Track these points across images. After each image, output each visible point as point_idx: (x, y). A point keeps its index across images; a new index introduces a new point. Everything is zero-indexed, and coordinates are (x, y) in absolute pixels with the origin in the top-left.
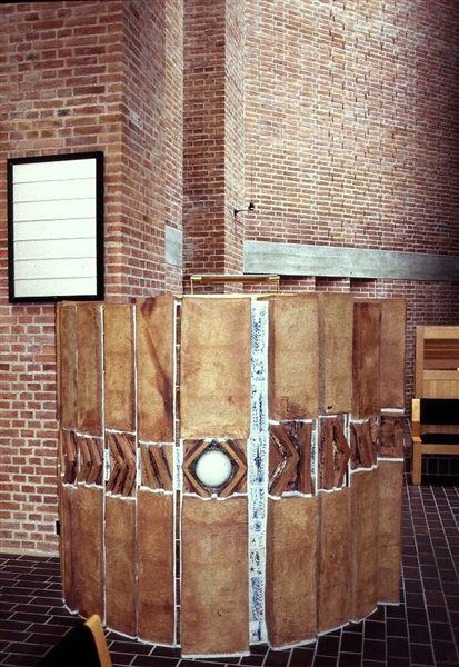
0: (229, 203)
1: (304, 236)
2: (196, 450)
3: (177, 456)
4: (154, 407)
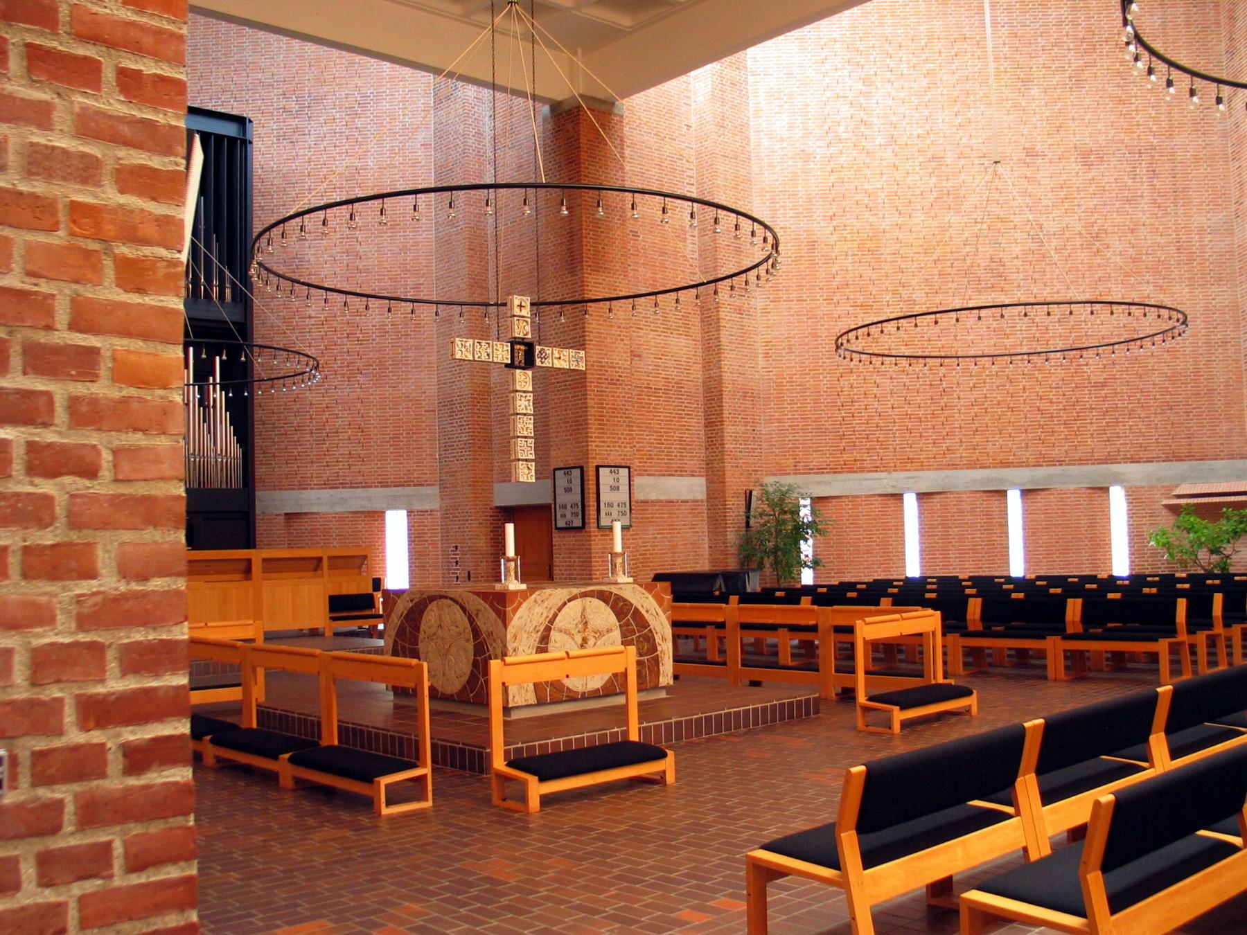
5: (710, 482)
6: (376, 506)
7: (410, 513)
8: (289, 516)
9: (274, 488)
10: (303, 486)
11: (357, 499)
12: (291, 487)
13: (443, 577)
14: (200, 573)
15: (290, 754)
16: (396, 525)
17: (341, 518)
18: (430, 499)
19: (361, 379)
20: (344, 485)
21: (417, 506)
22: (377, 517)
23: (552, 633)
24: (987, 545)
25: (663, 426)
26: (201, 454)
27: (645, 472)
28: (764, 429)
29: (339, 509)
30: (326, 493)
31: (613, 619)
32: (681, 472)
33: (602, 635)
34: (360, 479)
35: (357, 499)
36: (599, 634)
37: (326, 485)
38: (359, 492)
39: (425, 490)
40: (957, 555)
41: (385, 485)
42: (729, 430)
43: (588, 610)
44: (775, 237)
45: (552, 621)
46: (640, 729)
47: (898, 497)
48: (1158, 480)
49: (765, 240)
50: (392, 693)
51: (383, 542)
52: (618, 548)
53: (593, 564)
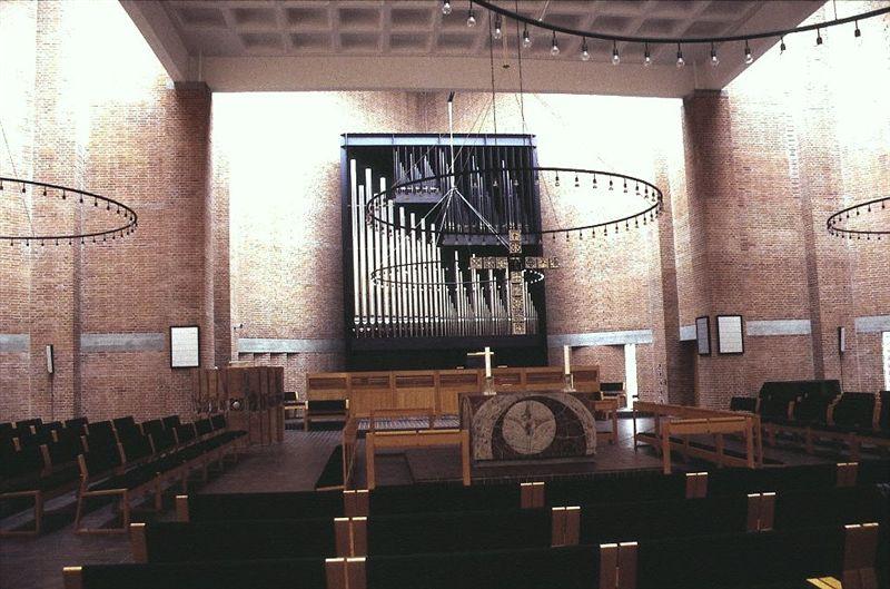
0: (232, 325)
1: (265, 335)
2: (232, 401)
3: (228, 403)
4: (222, 393)
5: (813, 322)
10: (580, 332)
12: (574, 333)
15: (810, 580)
23: (505, 421)
26: (394, 313)
27: (750, 319)
28: (854, 286)
31: (550, 413)
32: (789, 317)
33: (541, 422)
36: (539, 422)
37: (593, 330)
38: (610, 334)
39: (644, 332)
41: (622, 329)
42: (823, 288)
43: (531, 408)
44: (659, 192)
45: (505, 413)
47: (621, 347)
49: (653, 195)
50: (71, 417)
52: (489, 374)
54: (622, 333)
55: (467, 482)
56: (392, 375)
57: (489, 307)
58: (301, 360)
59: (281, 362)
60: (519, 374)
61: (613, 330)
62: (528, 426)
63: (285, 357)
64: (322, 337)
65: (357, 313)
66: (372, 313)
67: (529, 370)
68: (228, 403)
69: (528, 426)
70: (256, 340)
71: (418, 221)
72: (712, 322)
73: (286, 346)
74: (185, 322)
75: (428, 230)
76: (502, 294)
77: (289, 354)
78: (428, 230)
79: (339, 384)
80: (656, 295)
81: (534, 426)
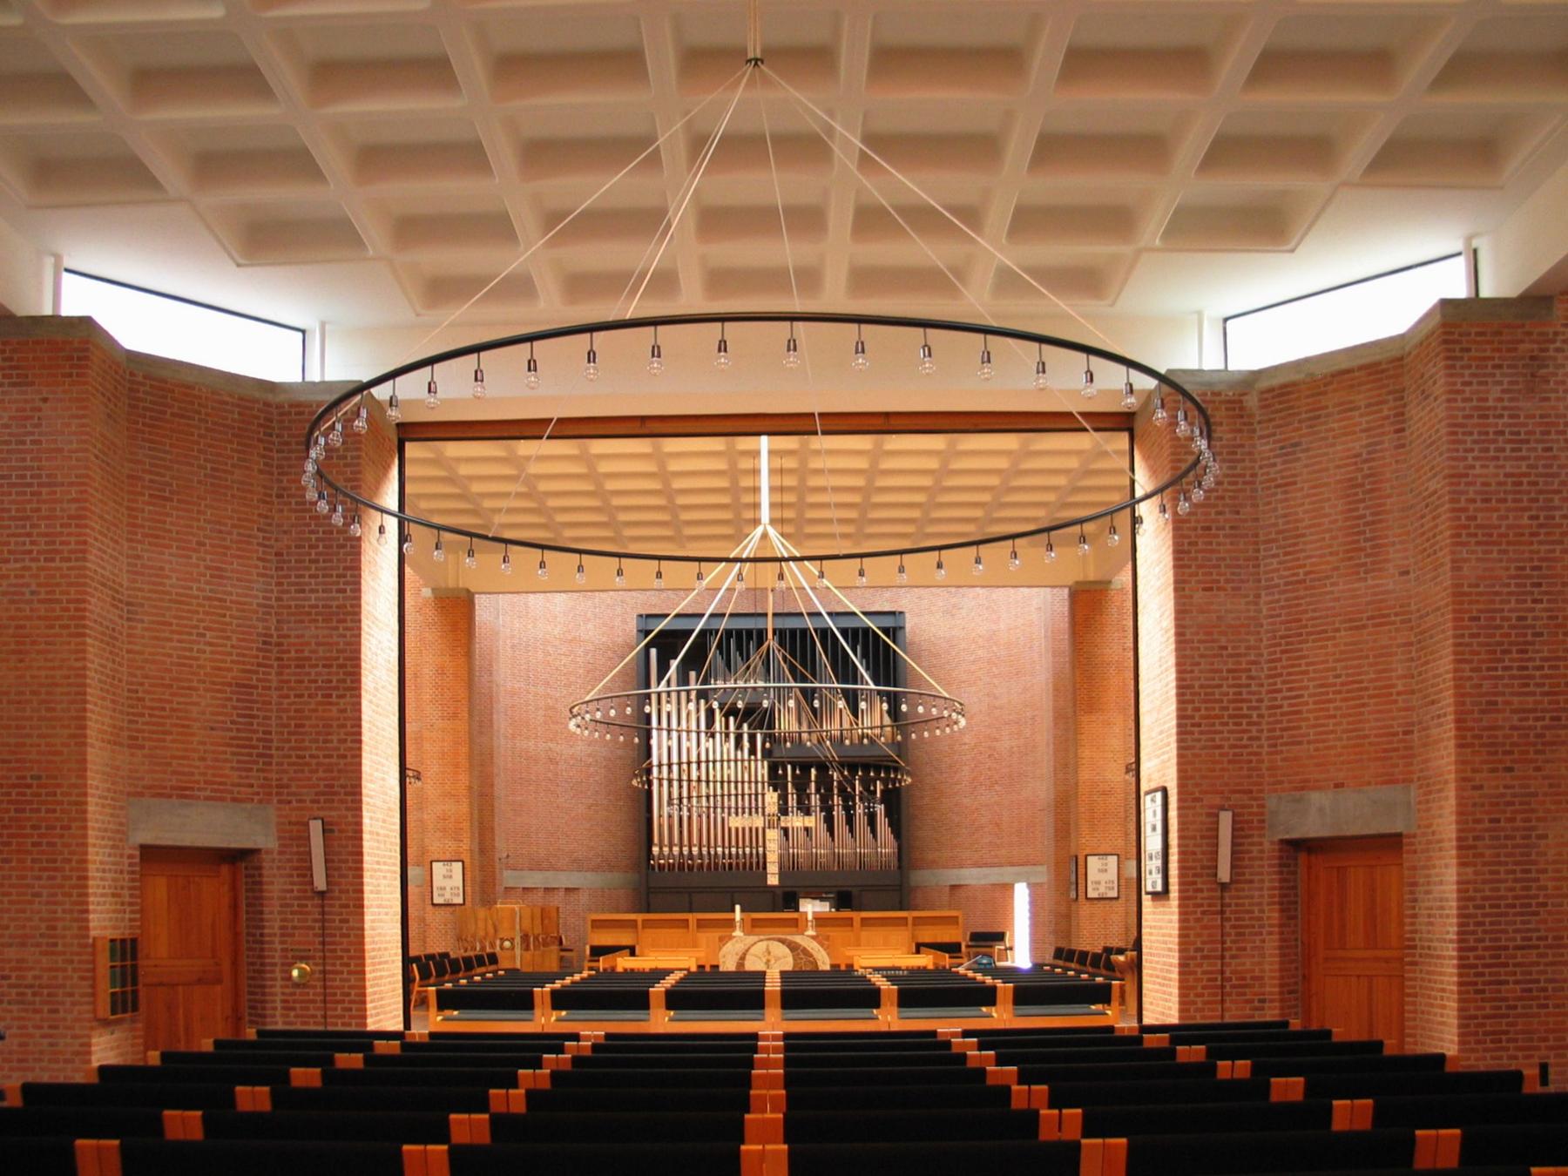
0: (497, 856)
1: (536, 866)
2: (502, 940)
3: (498, 942)
4: (491, 931)
6: (1007, 880)
7: (1029, 885)
8: (954, 887)
9: (944, 867)
11: (993, 875)
12: (954, 867)
13: (282, 935)
14: (597, 927)
16: (1021, 894)
17: (984, 888)
18: (1042, 874)
19: (997, 787)
20: (986, 865)
21: (1033, 880)
22: (1008, 888)
24: (1329, 701)
25: (72, 539)
29: (983, 882)
30: (975, 871)
31: (787, 950)
34: (996, 860)
35: (993, 875)
37: (977, 865)
38: (996, 870)
39: (1040, 868)
40: (1488, 877)
41: (1012, 865)
46: (825, 433)
48: (1164, 511)
51: (1013, 908)
53: (265, 879)
54: (1009, 869)
55: (782, 1056)
56: (692, 917)
57: (832, 835)
58: (584, 898)
59: (557, 900)
60: (852, 919)
61: (1001, 865)
62: (768, 961)
63: (562, 893)
64: (606, 866)
65: (656, 840)
66: (676, 840)
67: (865, 914)
68: (498, 942)
69: (768, 961)
70: (525, 873)
71: (739, 727)
72: (1081, 862)
73: (564, 880)
74: (448, 856)
75: (752, 739)
76: (386, 962)
77: (568, 890)
78: (752, 739)
79: (633, 924)
80: (1047, 821)
81: (773, 961)
